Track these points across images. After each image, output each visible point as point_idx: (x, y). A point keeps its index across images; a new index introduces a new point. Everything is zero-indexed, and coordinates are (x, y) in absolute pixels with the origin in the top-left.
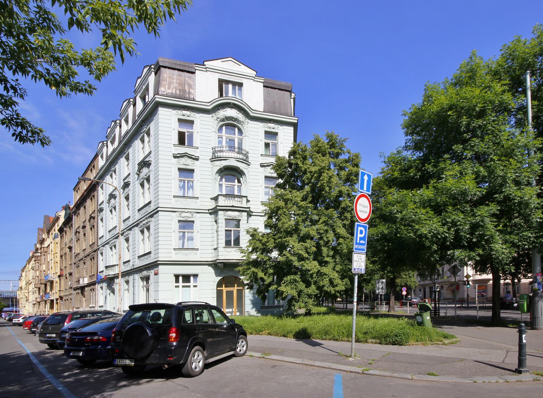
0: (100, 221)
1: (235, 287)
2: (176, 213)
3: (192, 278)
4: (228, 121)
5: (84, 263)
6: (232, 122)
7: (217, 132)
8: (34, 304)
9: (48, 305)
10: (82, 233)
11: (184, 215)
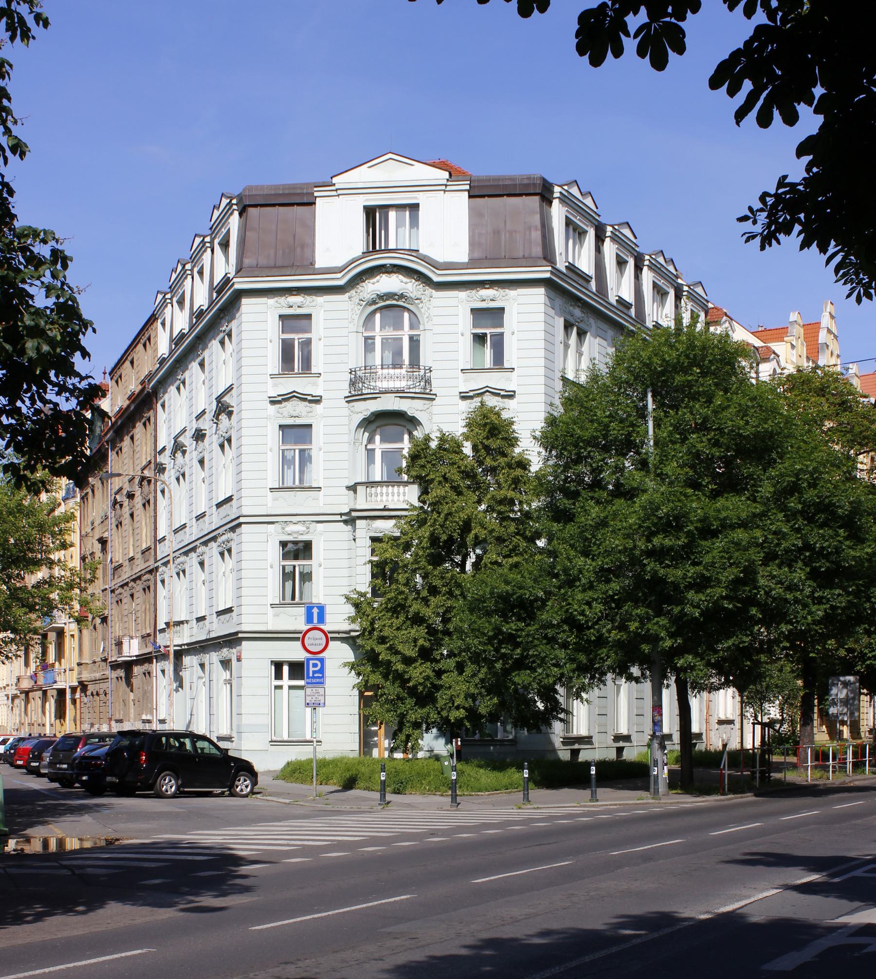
0: (159, 494)
2: (276, 525)
4: (385, 301)
5: (132, 596)
7: (361, 329)
8: (14, 697)
9: (51, 705)
10: (126, 510)
11: (291, 528)
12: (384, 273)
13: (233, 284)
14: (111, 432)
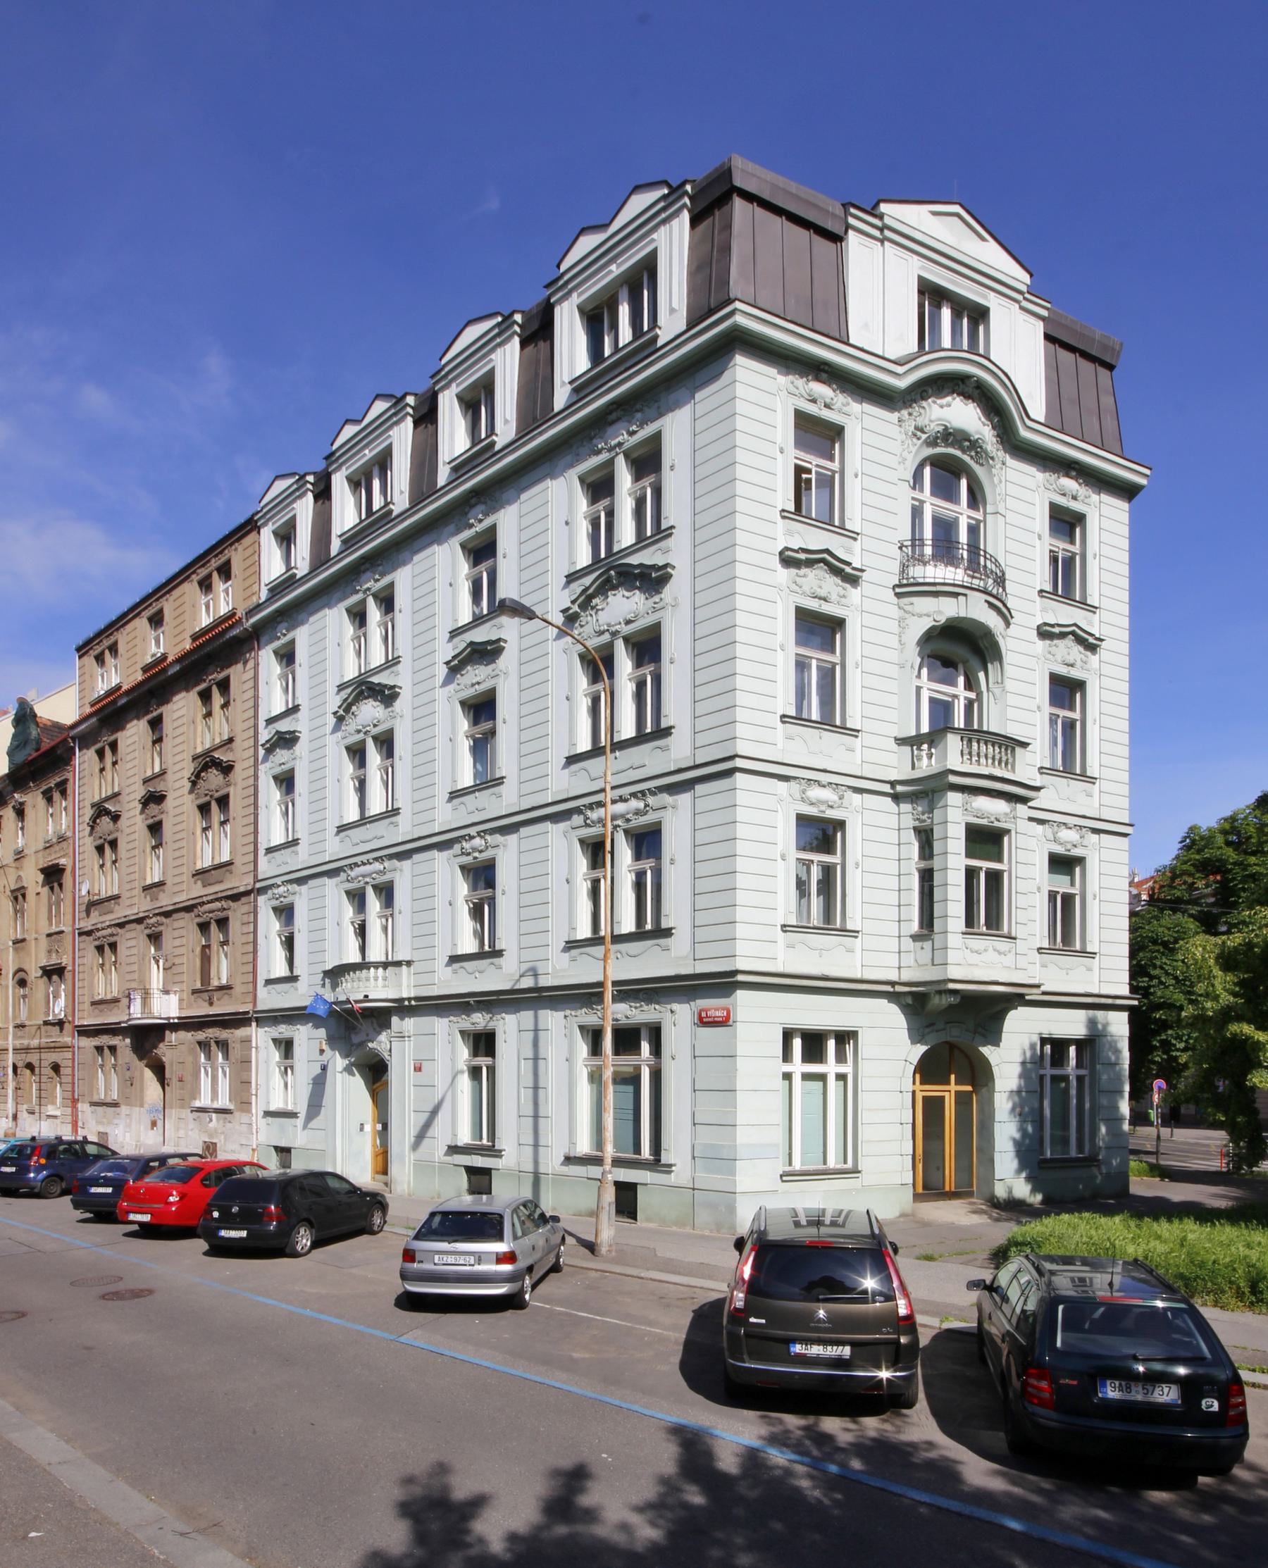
1: (948, 1083)
2: (793, 783)
3: (831, 1044)
4: (947, 446)
6: (958, 453)
11: (815, 793)
12: (959, 394)
13: (732, 313)
14: (94, 720)
